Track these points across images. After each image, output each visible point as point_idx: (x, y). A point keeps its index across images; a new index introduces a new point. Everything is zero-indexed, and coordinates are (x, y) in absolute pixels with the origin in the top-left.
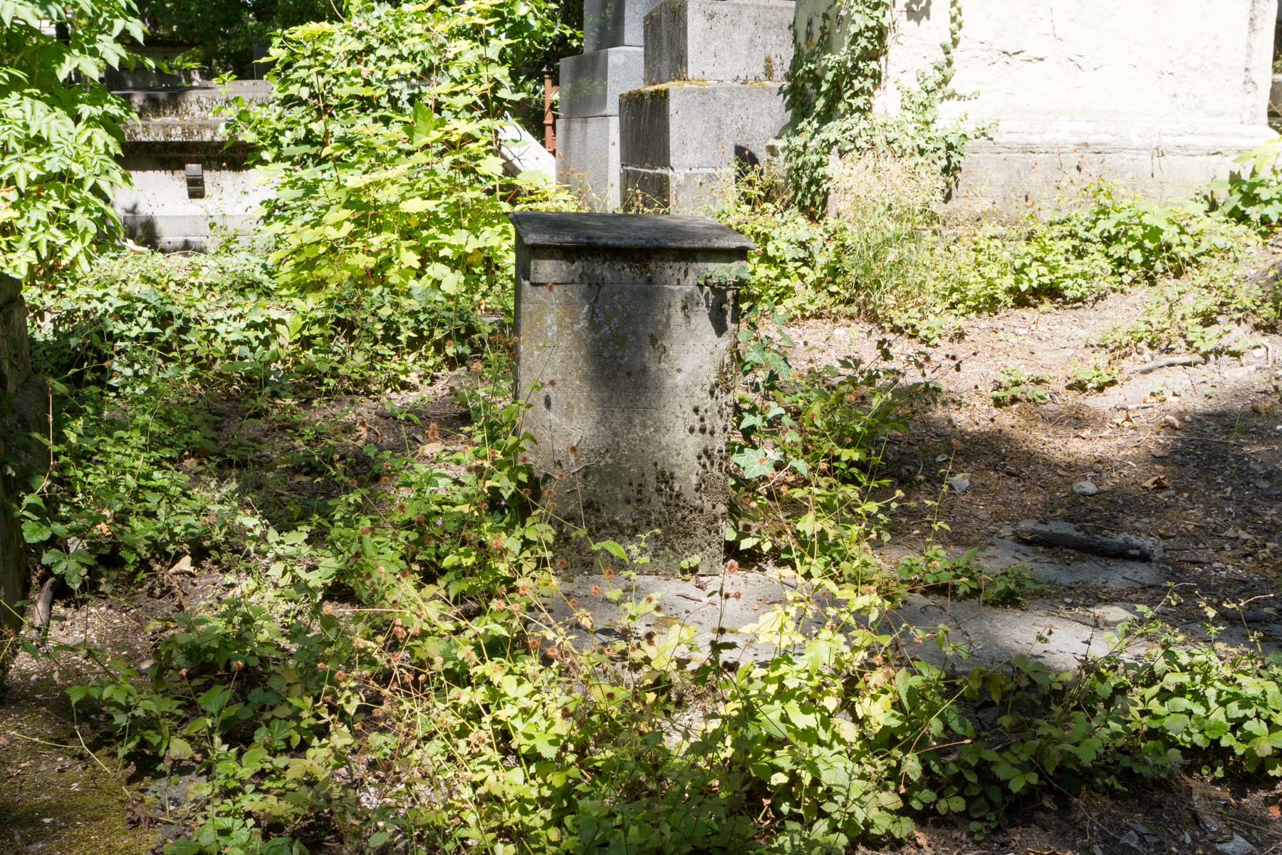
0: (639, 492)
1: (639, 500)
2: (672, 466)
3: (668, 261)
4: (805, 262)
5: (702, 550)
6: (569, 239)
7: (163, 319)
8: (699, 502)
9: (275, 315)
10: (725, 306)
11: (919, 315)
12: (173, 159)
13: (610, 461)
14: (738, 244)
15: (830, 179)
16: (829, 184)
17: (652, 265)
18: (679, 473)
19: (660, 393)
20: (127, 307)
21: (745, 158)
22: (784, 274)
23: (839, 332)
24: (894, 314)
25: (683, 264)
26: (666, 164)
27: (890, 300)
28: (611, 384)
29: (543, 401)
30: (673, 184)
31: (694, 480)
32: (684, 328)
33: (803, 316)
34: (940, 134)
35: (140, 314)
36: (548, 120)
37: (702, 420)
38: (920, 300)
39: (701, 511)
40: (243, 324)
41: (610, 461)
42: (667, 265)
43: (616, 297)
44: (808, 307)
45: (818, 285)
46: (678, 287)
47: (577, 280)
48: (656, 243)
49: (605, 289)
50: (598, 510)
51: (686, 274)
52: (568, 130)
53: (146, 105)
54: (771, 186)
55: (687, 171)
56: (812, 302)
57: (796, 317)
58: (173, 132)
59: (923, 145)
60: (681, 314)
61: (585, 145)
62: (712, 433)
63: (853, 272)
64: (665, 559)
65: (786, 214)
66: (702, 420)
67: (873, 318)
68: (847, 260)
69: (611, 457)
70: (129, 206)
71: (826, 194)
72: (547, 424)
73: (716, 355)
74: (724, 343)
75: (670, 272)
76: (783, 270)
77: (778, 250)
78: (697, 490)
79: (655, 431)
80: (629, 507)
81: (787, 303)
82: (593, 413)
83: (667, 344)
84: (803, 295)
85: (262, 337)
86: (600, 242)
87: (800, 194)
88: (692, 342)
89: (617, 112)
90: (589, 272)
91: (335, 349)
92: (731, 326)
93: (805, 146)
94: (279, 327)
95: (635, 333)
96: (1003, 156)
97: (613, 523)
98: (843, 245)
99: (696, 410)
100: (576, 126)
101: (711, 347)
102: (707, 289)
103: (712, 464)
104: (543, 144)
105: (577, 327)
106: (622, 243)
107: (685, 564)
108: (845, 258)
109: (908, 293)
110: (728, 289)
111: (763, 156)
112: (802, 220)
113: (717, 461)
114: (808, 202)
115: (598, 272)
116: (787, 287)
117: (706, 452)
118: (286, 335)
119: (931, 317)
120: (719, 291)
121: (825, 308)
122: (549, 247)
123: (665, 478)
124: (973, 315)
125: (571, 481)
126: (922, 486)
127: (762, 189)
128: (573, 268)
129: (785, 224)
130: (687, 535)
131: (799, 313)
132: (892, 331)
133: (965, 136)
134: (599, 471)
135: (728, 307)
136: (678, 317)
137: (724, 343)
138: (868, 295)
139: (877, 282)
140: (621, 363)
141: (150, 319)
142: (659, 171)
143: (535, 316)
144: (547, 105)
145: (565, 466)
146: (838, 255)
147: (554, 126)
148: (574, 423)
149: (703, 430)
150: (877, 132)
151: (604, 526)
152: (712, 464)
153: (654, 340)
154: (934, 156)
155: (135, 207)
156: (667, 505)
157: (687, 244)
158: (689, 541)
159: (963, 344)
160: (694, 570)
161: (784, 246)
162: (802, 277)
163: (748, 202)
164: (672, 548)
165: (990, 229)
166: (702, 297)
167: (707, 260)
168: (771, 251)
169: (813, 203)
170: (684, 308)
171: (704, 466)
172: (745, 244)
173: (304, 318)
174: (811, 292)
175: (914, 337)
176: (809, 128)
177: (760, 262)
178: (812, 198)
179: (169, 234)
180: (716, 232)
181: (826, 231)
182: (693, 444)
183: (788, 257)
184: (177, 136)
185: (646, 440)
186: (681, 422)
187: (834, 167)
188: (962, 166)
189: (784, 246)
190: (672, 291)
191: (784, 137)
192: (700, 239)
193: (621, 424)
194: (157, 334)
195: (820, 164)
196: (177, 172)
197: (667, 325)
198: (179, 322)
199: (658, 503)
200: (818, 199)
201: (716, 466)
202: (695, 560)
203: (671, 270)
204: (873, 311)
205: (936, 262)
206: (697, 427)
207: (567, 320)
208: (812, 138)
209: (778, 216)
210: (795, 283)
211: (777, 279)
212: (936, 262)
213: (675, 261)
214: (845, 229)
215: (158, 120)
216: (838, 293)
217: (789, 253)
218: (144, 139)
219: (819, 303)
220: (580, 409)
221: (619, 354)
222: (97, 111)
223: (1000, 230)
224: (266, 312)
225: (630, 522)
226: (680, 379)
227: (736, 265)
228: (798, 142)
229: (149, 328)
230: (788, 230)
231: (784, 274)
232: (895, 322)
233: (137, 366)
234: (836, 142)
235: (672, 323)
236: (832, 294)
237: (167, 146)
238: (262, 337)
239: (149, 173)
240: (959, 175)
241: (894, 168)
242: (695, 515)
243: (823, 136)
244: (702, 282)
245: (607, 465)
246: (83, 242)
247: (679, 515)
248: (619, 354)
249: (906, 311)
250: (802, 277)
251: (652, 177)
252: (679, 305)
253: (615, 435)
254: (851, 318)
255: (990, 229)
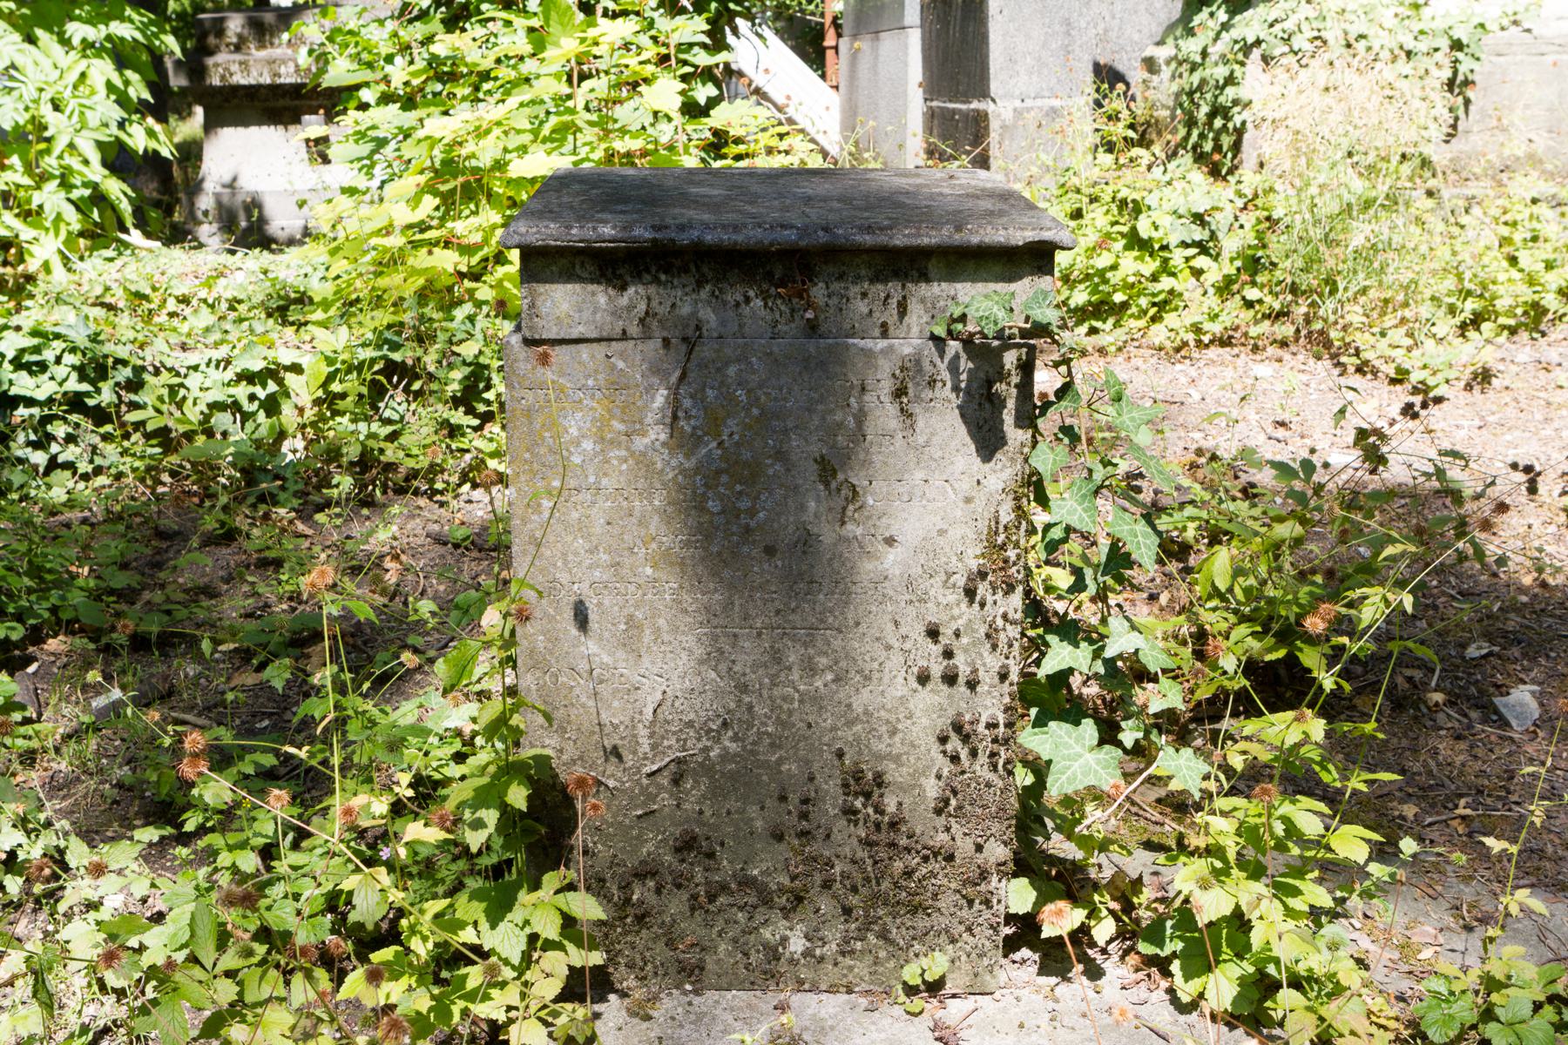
0: (804, 816)
1: (804, 834)
2: (880, 757)
3: (858, 279)
4: (1203, 248)
5: (953, 941)
6: (607, 231)
7: (95, 369)
8: (943, 837)
9: (286, 357)
10: (999, 387)
11: (1410, 342)
12: (286, 109)
13: (734, 747)
14: (1030, 235)
15: (1248, 104)
16: (1246, 115)
17: (818, 292)
18: (893, 773)
19: (847, 593)
20: (37, 350)
21: (1107, 76)
22: (1166, 269)
23: (1264, 370)
24: (1362, 339)
25: (894, 288)
26: (984, 94)
27: (1355, 315)
28: (726, 574)
29: (569, 614)
30: (994, 125)
31: (932, 789)
32: (899, 442)
33: (1199, 343)
34: (1440, 24)
35: (58, 360)
36: (830, 40)
37: (948, 654)
38: (1407, 313)
39: (950, 858)
40: (230, 374)
41: (734, 747)
42: (855, 290)
43: (732, 371)
44: (1207, 326)
45: (1226, 288)
46: (882, 344)
47: (634, 330)
48: (823, 237)
49: (705, 351)
50: (711, 855)
51: (903, 310)
52: (855, 56)
53: (246, 32)
54: (1148, 123)
55: (1018, 103)
56: (1214, 317)
57: (1185, 344)
58: (283, 70)
59: (1410, 44)
60: (892, 409)
61: (876, 73)
62: (972, 685)
63: (1288, 264)
64: (869, 959)
65: (1171, 166)
66: (948, 654)
67: (1321, 344)
68: (1277, 245)
69: (735, 739)
70: (227, 179)
71: (1240, 132)
72: (583, 666)
73: (979, 504)
74: (1001, 474)
75: (862, 307)
76: (1166, 261)
77: (1156, 228)
78: (938, 812)
79: (837, 680)
80: (782, 847)
81: (1170, 319)
82: (690, 640)
83: (859, 480)
84: (1199, 305)
85: (262, 394)
86: (684, 239)
87: (1195, 133)
88: (919, 475)
89: (918, 21)
90: (662, 310)
91: (387, 414)
92: (1016, 436)
93: (1204, 54)
94: (290, 379)
95: (780, 455)
96: (1550, 58)
97: (747, 883)
98: (1268, 219)
99: (933, 633)
100: (863, 44)
101: (966, 486)
102: (954, 346)
103: (974, 753)
104: (823, 76)
105: (640, 443)
106: (739, 238)
107: (911, 974)
108: (1271, 238)
109: (1386, 301)
110: (1006, 347)
111: (1136, 75)
112: (1199, 176)
113: (985, 747)
114: (1208, 146)
115: (685, 310)
116: (1171, 292)
117: (958, 727)
118: (302, 390)
119: (1430, 344)
120: (984, 352)
121: (1236, 329)
122: (560, 252)
123: (865, 784)
124: (1502, 339)
125: (644, 790)
126: (1441, 717)
127: (1132, 126)
128: (624, 301)
129: (1169, 183)
130: (914, 910)
131: (1190, 337)
132: (1359, 370)
133: (1482, 26)
134: (707, 768)
135: (1008, 391)
136: (884, 415)
137: (1001, 474)
138: (1313, 304)
139: (1331, 283)
140: (763, 520)
141: (74, 367)
142: (975, 105)
143: (539, 421)
144: (828, 21)
145: (629, 760)
146: (1260, 235)
147: (836, 48)
148: (646, 661)
149: (950, 679)
150: (1329, 24)
151: (724, 888)
152: (974, 753)
153: (827, 470)
154: (1428, 63)
155: (235, 179)
156: (868, 843)
157: (901, 238)
158: (921, 922)
159: (1491, 394)
160: (934, 988)
161: (1166, 221)
162: (1197, 273)
163: (1110, 147)
164: (884, 935)
165: (1524, 185)
166: (943, 366)
167: (952, 277)
168: (1144, 229)
169: (1217, 148)
170: (900, 393)
171: (955, 759)
172: (1047, 235)
173: (330, 361)
174: (1213, 301)
175: (1400, 382)
176: (1211, 23)
177: (1127, 248)
178: (1216, 140)
179: (282, 220)
180: (987, 204)
181: (1240, 195)
182: (927, 711)
183: (1173, 240)
184: (288, 77)
185: (816, 700)
186: (897, 659)
187: (1254, 83)
188: (1475, 77)
189: (1166, 221)
190: (868, 354)
191: (1170, 41)
192: (936, 225)
193: (755, 666)
194: (88, 394)
195: (1230, 80)
196: (292, 128)
197: (859, 435)
198: (125, 373)
199: (847, 840)
200: (1226, 141)
201: (983, 758)
202: (936, 964)
203: (864, 302)
204: (1321, 332)
205: (1431, 250)
206: (937, 670)
207: (618, 426)
208: (1216, 39)
209: (1157, 171)
210: (1184, 283)
211: (1154, 278)
212: (1431, 250)
213: (874, 279)
214: (1271, 189)
215: (263, 54)
216: (1260, 301)
217: (1174, 232)
218: (243, 82)
219: (1227, 319)
220: (657, 631)
221: (744, 504)
222: (95, 33)
223: (1544, 188)
224: (271, 354)
225: (786, 881)
226: (892, 561)
227: (1024, 288)
228: (1191, 47)
229: (73, 385)
230: (1175, 192)
231: (1166, 269)
232: (1364, 355)
233: (54, 448)
234: (1258, 42)
235: (870, 430)
236: (1249, 304)
237: (276, 90)
238: (262, 394)
239: (254, 129)
240: (1470, 93)
241: (1360, 87)
242: (934, 865)
243: (1235, 33)
244: (940, 331)
245: (725, 757)
246: (57, 234)
247: (898, 865)
248: (744, 504)
249: (1383, 334)
250: (1197, 273)
251: (965, 115)
252: (887, 386)
253: (743, 688)
254: (1284, 344)
255: (1524, 185)
